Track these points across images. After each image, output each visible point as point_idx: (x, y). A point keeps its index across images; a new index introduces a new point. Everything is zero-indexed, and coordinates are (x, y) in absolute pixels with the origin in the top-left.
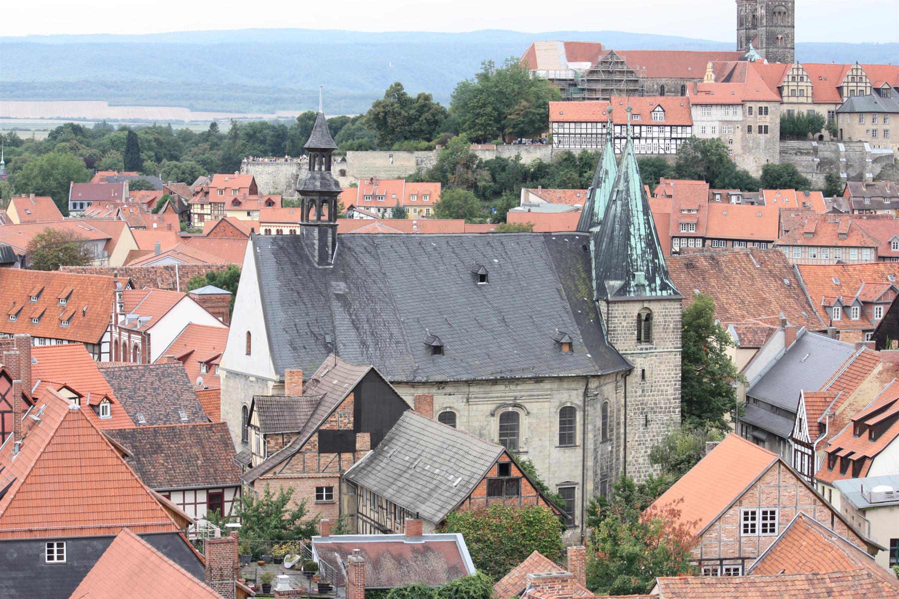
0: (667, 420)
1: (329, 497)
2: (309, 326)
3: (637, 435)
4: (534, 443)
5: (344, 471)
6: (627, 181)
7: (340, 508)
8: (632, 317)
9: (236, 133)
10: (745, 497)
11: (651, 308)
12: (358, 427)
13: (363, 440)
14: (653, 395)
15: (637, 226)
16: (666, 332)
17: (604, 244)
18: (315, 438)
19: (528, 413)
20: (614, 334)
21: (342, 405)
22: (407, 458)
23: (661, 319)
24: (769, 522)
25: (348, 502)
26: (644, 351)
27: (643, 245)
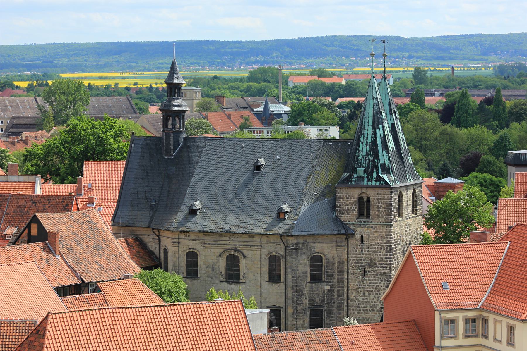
2: (145, 193)
3: (357, 281)
4: (249, 277)
8: (353, 199)
14: (370, 254)
15: (366, 137)
16: (379, 211)
20: (340, 210)
21: (22, 235)
26: (363, 223)
27: (368, 149)
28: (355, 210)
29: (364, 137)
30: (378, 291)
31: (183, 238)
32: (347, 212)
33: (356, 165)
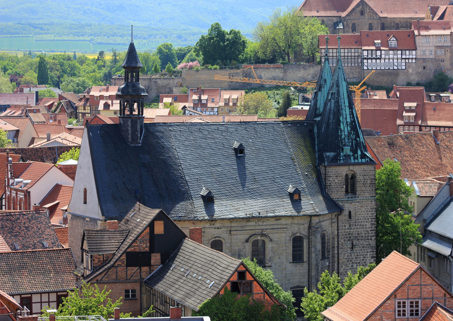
0: (366, 245)
1: (134, 296)
3: (346, 255)
5: (144, 279)
6: (338, 86)
7: (141, 303)
8: (342, 176)
9: (115, 59)
10: (398, 292)
11: (355, 170)
12: (152, 250)
13: (156, 258)
14: (357, 228)
15: (345, 117)
16: (365, 186)
17: (323, 129)
18: (124, 257)
19: (271, 240)
20: (330, 188)
21: (142, 235)
22: (182, 270)
23: (361, 178)
24: (414, 309)
25: (146, 299)
27: (349, 129)
28: (343, 187)
29: (343, 117)
30: (365, 262)
31: (208, 226)
32: (336, 190)
33: (340, 144)
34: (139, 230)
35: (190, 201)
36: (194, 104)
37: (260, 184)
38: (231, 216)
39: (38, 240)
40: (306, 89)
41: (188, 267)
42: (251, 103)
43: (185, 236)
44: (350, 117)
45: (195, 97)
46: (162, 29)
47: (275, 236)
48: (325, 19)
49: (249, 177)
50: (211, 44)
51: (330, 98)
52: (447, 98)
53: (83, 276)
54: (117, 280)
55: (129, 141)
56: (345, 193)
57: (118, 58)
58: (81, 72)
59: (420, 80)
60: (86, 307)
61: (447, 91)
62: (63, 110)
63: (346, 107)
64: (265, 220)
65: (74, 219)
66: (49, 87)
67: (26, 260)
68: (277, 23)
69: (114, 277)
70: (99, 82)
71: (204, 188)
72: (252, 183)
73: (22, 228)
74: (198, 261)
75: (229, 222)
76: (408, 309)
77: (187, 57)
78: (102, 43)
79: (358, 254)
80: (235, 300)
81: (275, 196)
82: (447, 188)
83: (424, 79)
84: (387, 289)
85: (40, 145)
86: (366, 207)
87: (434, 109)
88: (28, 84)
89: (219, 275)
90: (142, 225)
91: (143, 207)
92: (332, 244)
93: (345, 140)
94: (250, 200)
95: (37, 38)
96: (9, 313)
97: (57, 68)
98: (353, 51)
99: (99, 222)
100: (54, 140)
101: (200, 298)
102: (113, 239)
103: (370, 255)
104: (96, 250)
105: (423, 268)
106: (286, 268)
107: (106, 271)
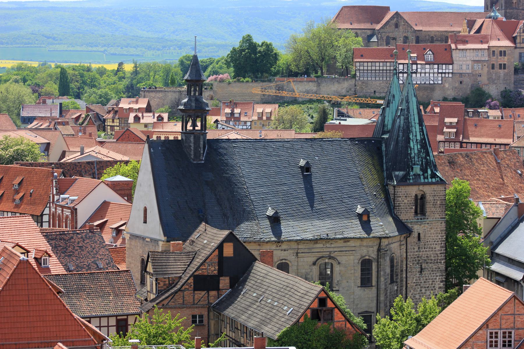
0: (436, 268)
1: (201, 321)
3: (415, 279)
5: (211, 304)
6: (408, 102)
7: (208, 329)
8: (411, 197)
9: (136, 70)
10: (490, 321)
11: (424, 190)
12: (221, 273)
13: (224, 282)
14: (426, 251)
15: (414, 134)
16: (435, 207)
17: (392, 146)
18: (191, 280)
19: (339, 263)
20: (399, 209)
21: (210, 257)
22: (255, 295)
24: (507, 339)
25: (214, 325)
27: (419, 147)
29: (413, 134)
30: (434, 287)
31: (274, 248)
32: (405, 211)
33: (410, 162)
34: (206, 253)
35: (255, 222)
36: (226, 118)
37: (327, 204)
38: (299, 238)
39: (93, 260)
40: (340, 104)
41: (261, 292)
42: (287, 117)
43: (256, 259)
44: (420, 135)
45: (228, 110)
46: (176, 40)
47: (343, 259)
48: (359, 32)
49: (317, 197)
50: (243, 56)
51: (399, 114)
52: (485, 114)
53: (146, 300)
54: (184, 305)
55: (191, 158)
56: (415, 214)
57: (138, 69)
58: (101, 83)
59: (456, 94)
60: (155, 334)
61: (485, 106)
62: (91, 123)
63: (416, 124)
64: (333, 242)
65: (132, 239)
66: (70, 98)
67: (84, 282)
68: (311, 35)
69: (181, 301)
70: (121, 94)
71: (270, 208)
72: (320, 203)
73: (76, 248)
74: (272, 286)
75: (296, 243)
76: (500, 340)
77: (209, 69)
78: (115, 54)
79: (427, 278)
80: (315, 328)
81: (342, 217)
82: (515, 210)
83: (460, 94)
84: (478, 319)
85: (74, 159)
86: (435, 229)
87: (476, 125)
88: (49, 95)
89: (298, 301)
90: (210, 247)
91: (209, 228)
92: (401, 268)
93: (415, 159)
94: (317, 221)
95: (50, 48)
96: (96, 344)
97: (77, 79)
98: (388, 64)
99: (161, 243)
100: (88, 154)
101: (278, 326)
102: (179, 261)
103: (439, 279)
104: (161, 272)
105: (517, 297)
106: (354, 292)
107: (173, 295)
